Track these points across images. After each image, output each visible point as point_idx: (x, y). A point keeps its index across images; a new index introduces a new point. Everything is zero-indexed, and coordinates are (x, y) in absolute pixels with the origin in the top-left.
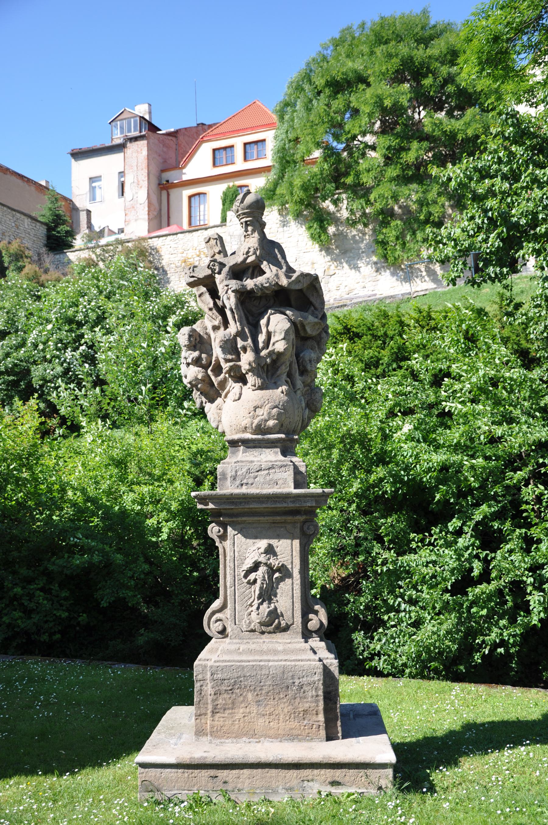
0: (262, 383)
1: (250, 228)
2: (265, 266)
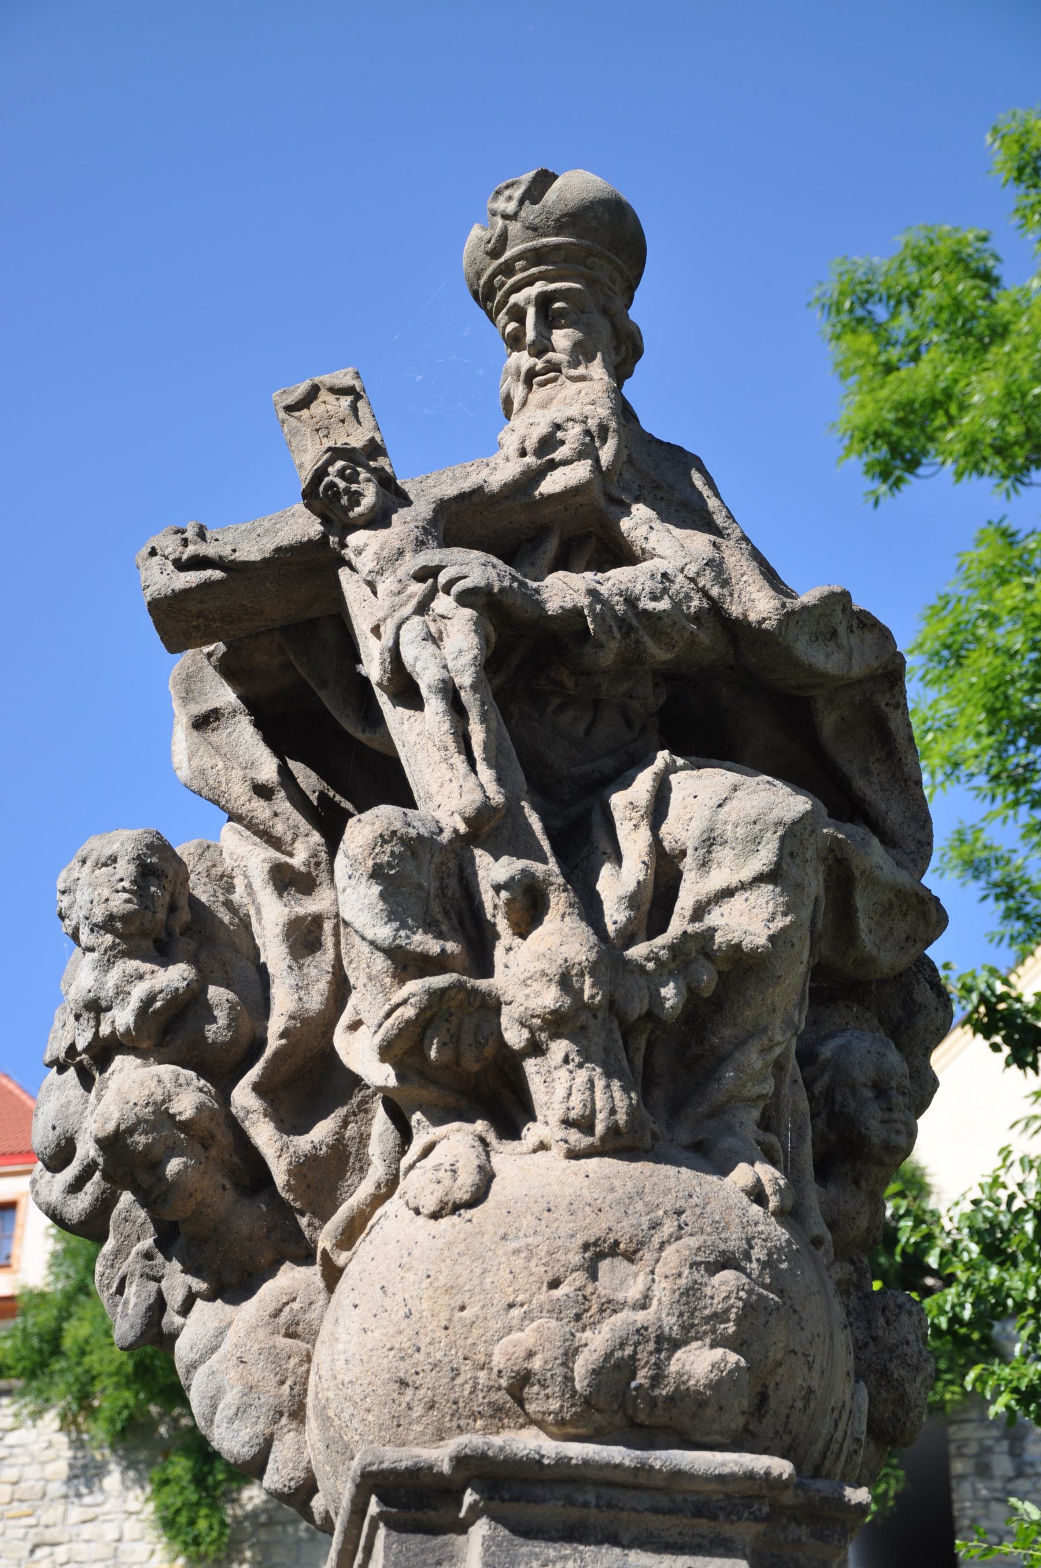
0: (632, 1112)
1: (562, 338)
2: (639, 523)
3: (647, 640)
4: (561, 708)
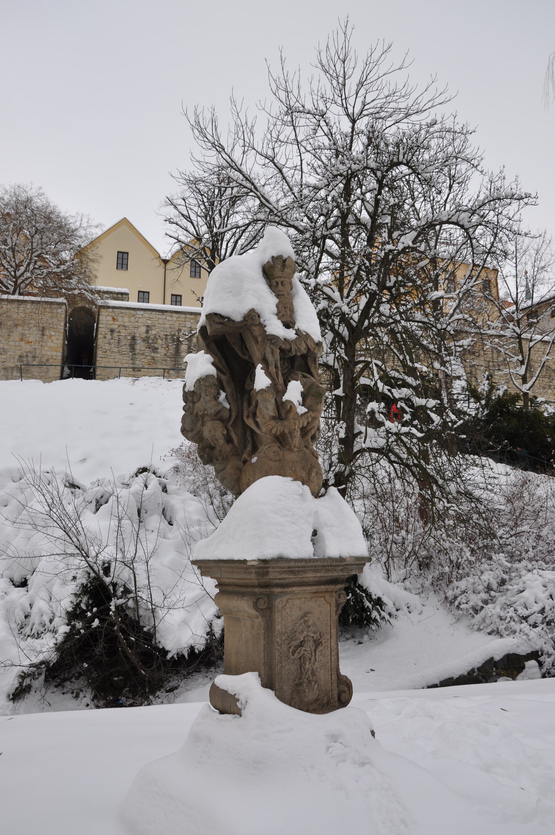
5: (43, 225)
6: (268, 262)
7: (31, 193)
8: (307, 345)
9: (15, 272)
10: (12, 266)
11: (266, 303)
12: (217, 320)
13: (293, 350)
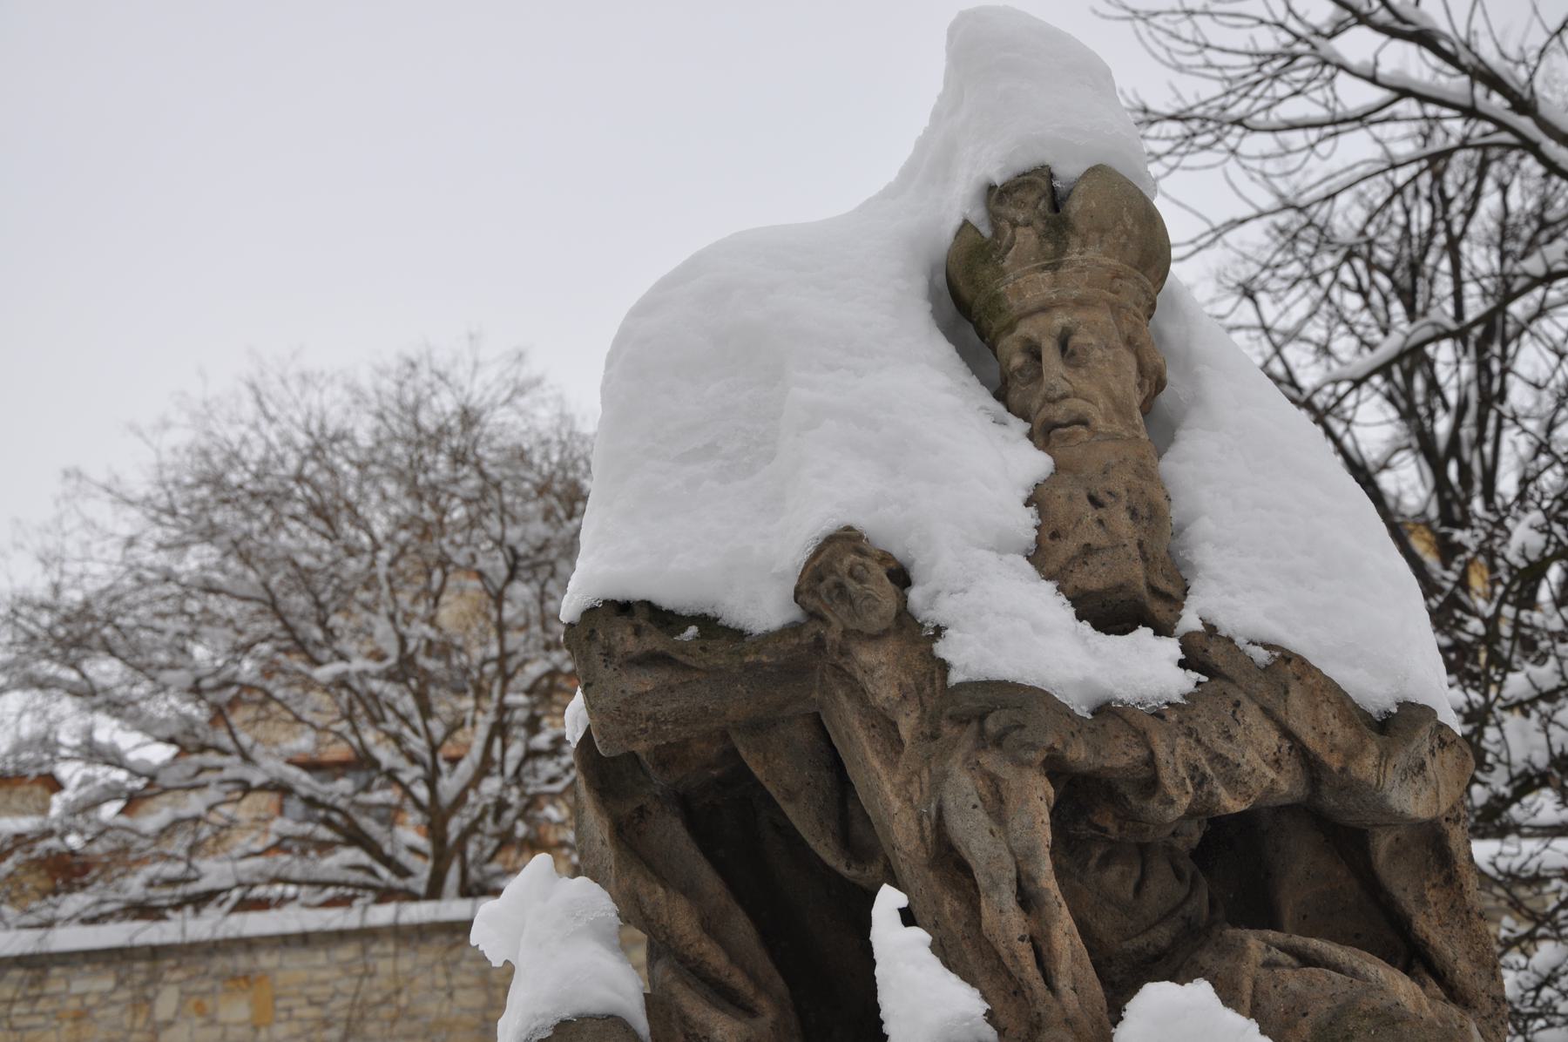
3: (1222, 792)
4: (1105, 862)
5: (539, 529)
6: (966, 224)
7: (481, 388)
8: (1287, 733)
9: (431, 781)
10: (413, 759)
11: (955, 483)
12: (626, 641)
13: (1172, 773)
